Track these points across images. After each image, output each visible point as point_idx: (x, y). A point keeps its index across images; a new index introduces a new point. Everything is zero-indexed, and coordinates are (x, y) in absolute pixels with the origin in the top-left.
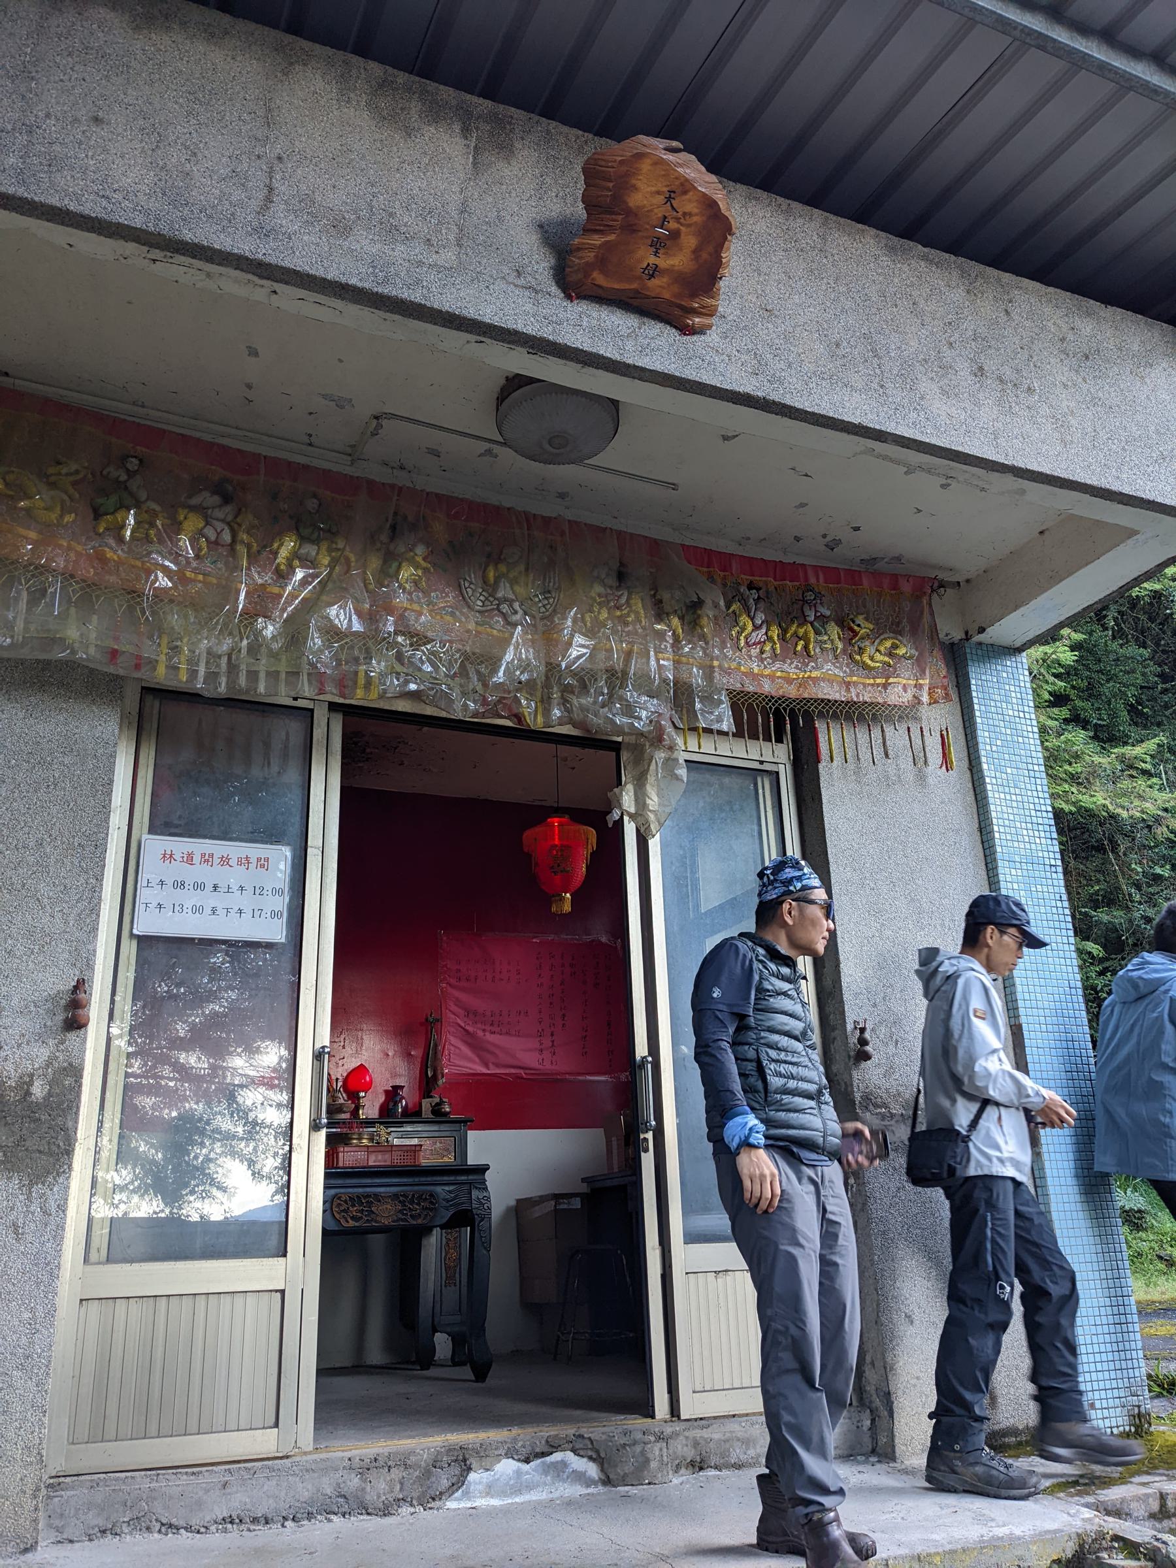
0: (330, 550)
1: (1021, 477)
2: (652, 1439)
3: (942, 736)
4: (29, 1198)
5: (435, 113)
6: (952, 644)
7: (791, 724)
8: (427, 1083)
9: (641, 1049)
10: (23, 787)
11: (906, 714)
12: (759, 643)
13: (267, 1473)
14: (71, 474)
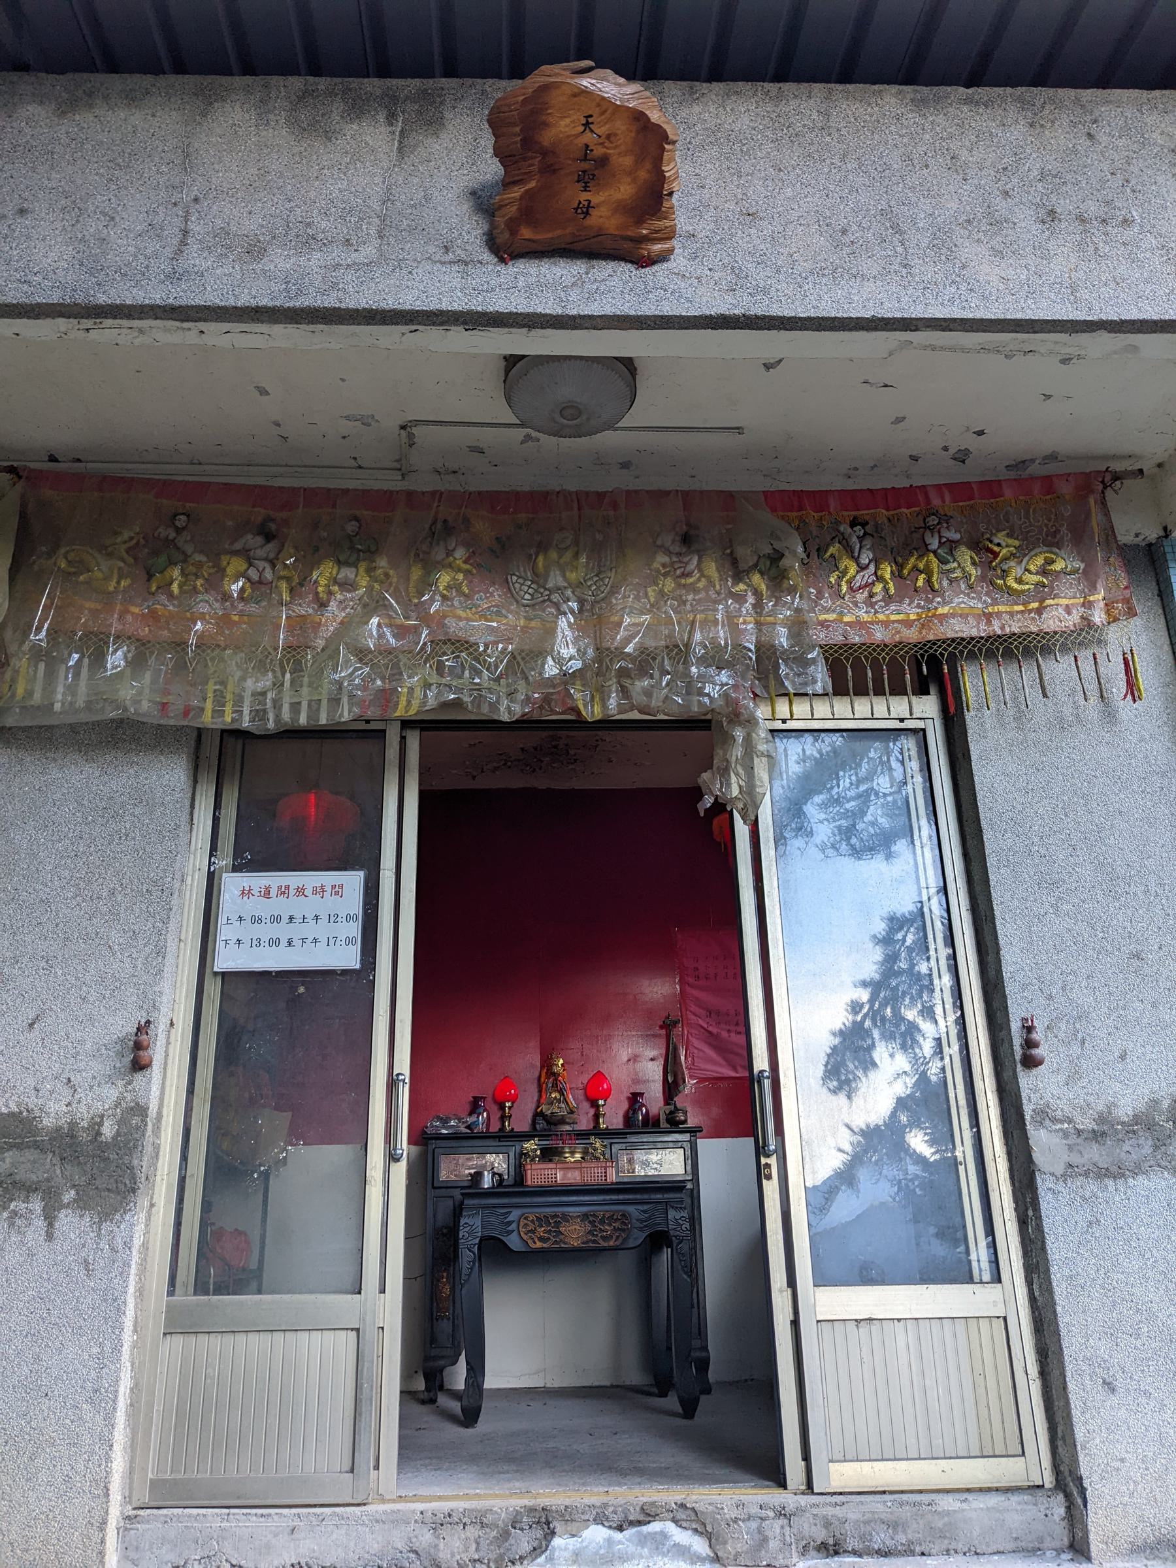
0: (369, 571)
1: (1119, 332)
2: (771, 1514)
3: (1126, 661)
4: (99, 1235)
5: (358, 109)
6: (1150, 545)
7: (931, 669)
9: (761, 1063)
10: (99, 841)
11: (1086, 635)
12: (866, 585)
13: (336, 1520)
14: (125, 542)
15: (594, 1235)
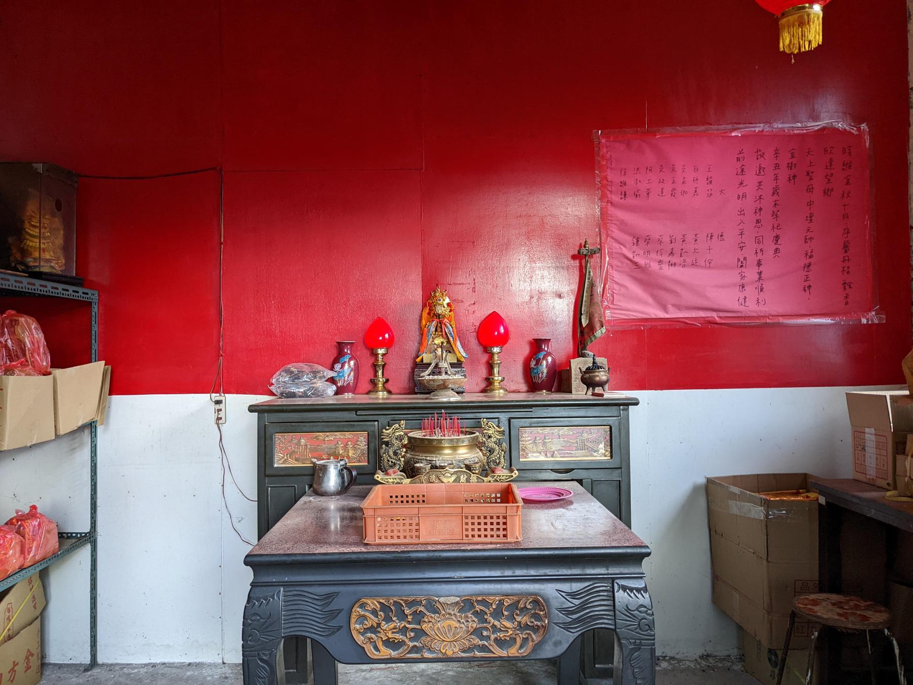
8: (582, 332)
15: (482, 637)
